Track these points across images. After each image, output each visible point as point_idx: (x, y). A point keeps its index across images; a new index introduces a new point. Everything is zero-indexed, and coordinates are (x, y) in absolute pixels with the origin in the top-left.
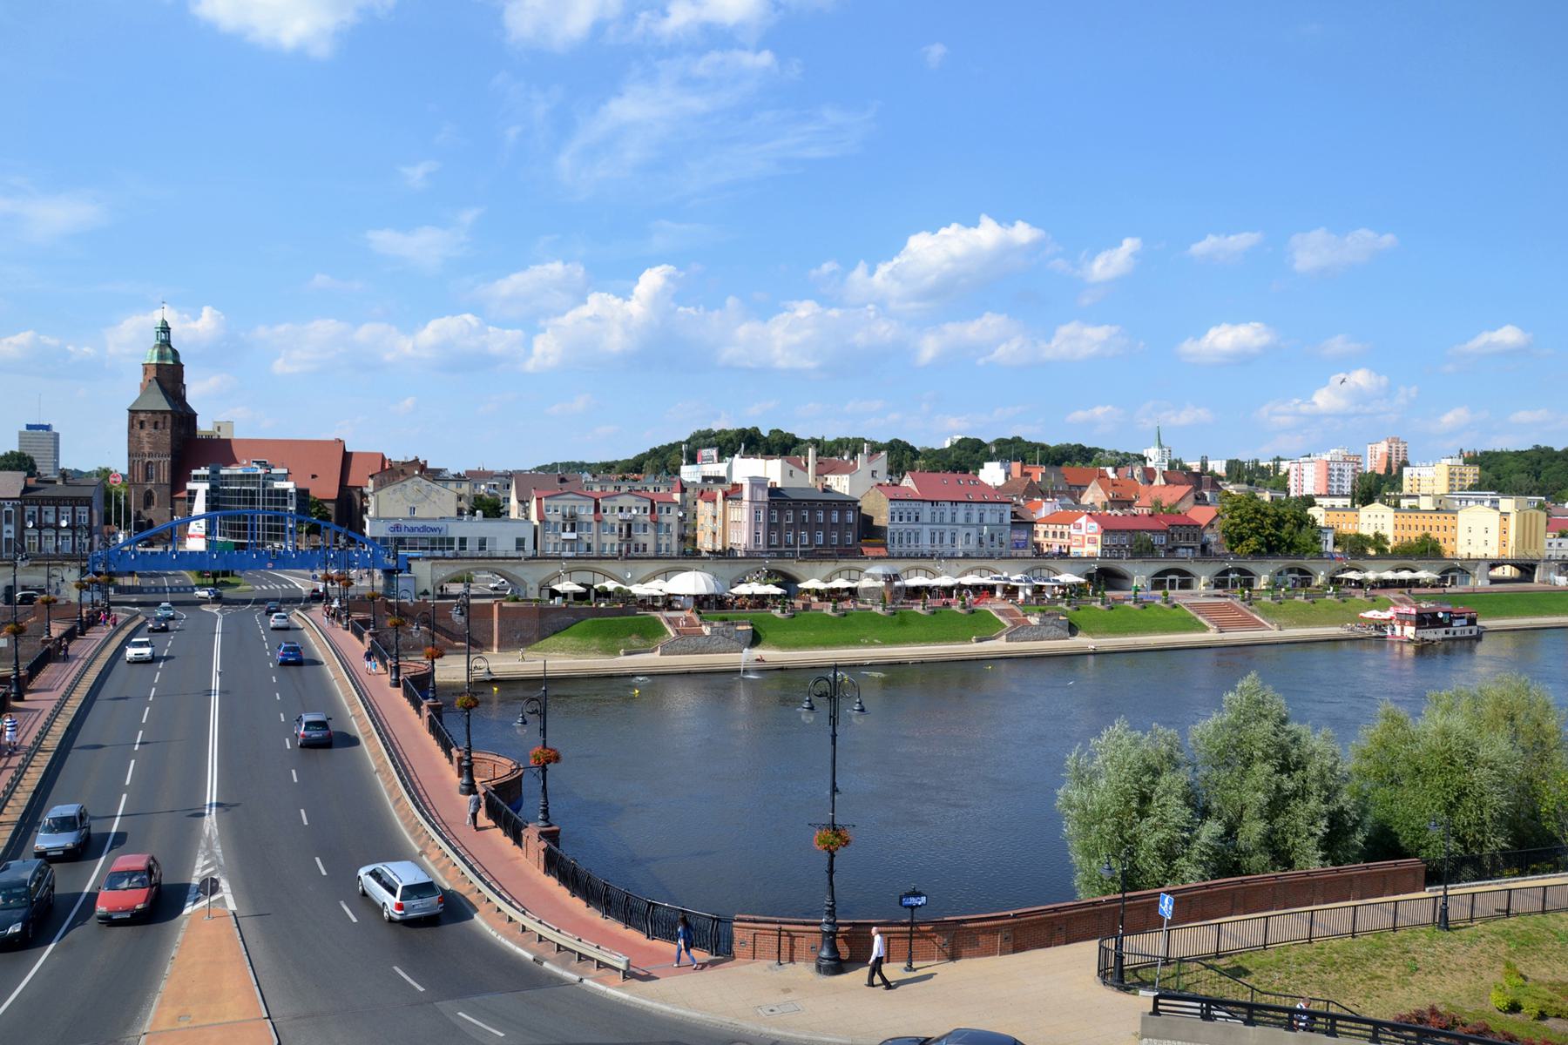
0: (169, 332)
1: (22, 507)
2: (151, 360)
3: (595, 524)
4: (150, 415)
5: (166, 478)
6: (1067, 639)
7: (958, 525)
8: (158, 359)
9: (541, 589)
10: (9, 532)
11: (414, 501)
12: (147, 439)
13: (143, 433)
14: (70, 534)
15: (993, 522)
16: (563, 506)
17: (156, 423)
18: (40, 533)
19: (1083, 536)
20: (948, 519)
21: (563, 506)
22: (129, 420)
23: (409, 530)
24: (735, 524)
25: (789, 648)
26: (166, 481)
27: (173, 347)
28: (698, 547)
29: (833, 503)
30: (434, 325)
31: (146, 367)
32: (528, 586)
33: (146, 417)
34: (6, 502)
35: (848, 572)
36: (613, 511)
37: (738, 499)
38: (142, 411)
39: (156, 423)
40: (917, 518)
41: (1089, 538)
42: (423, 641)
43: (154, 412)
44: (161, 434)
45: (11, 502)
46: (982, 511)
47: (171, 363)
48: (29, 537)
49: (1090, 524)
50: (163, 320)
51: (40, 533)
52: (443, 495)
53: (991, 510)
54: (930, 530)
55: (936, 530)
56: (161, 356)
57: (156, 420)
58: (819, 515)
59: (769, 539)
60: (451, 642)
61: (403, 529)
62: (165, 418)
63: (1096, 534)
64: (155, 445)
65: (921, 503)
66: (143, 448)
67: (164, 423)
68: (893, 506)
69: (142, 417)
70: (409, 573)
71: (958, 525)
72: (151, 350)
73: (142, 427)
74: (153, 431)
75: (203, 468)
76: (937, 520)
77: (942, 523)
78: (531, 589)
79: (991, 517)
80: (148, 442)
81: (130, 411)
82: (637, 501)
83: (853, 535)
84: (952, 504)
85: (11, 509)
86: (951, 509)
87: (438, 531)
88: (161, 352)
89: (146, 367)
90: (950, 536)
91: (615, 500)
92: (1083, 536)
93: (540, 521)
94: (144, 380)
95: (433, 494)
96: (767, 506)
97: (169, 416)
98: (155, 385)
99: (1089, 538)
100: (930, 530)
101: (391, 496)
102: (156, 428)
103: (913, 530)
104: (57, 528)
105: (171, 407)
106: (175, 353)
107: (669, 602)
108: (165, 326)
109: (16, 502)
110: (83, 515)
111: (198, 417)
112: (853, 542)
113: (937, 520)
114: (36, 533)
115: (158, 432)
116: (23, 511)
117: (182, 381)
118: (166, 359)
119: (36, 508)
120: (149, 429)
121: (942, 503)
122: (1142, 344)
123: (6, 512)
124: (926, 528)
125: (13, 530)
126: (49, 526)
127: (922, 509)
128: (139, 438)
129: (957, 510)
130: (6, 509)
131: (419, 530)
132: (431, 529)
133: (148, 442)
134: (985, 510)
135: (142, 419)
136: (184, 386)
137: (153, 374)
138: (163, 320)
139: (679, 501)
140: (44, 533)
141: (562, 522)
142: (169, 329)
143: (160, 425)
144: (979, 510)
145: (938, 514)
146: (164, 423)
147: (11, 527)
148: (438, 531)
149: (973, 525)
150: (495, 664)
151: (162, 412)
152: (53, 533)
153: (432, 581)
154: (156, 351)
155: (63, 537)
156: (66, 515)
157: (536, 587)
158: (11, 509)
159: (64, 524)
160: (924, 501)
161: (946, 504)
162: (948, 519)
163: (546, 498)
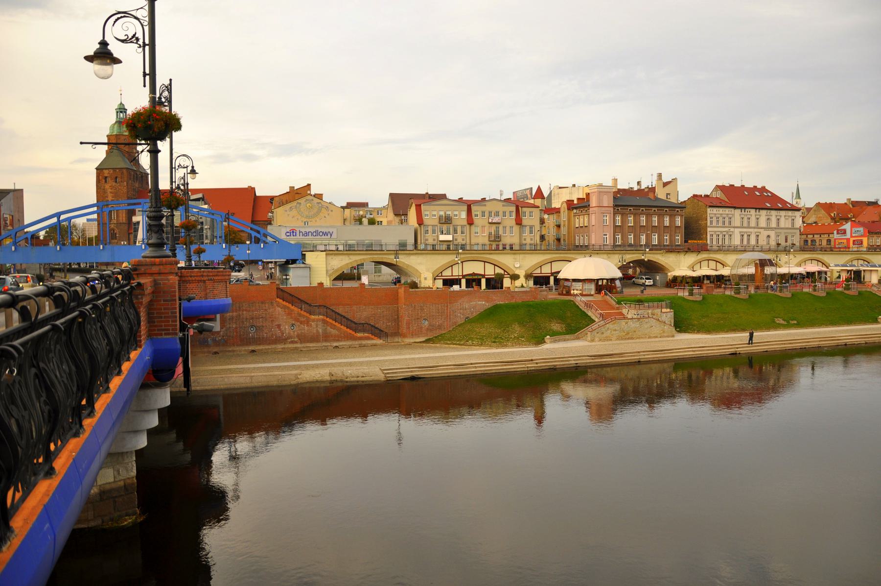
2: (113, 133)
5: (124, 219)
6: (673, 336)
7: (761, 228)
9: (435, 279)
11: (307, 217)
12: (110, 190)
13: (107, 186)
15: (787, 226)
19: (848, 240)
20: (753, 223)
23: (303, 235)
24: (581, 230)
25: (826, 325)
26: (124, 221)
32: (423, 276)
35: (707, 261)
36: (483, 215)
37: (585, 207)
40: (730, 223)
41: (854, 241)
42: (320, 331)
43: (114, 169)
44: (119, 186)
49: (854, 229)
50: (121, 103)
53: (785, 216)
54: (740, 232)
57: (116, 176)
58: (654, 219)
59: (615, 239)
60: (353, 333)
61: (298, 234)
63: (862, 236)
64: (116, 195)
65: (733, 210)
66: (107, 197)
69: (106, 173)
70: (303, 263)
71: (761, 228)
74: (114, 184)
76: (745, 224)
77: (757, 227)
78: (426, 279)
79: (785, 222)
80: (111, 192)
82: (503, 206)
83: (681, 237)
87: (329, 235)
90: (755, 238)
91: (485, 205)
92: (848, 240)
95: (323, 210)
96: (612, 209)
99: (854, 241)
100: (740, 232)
101: (288, 212)
102: (116, 182)
103: (721, 232)
107: (233, 376)
108: (122, 107)
112: (681, 242)
113: (745, 224)
120: (111, 182)
121: (749, 210)
124: (737, 231)
127: (733, 215)
128: (104, 189)
131: (312, 234)
132: (323, 233)
133: (111, 192)
134: (781, 216)
135: (106, 175)
138: (121, 103)
142: (127, 110)
144: (776, 216)
145: (745, 219)
148: (329, 235)
149: (772, 229)
151: (121, 169)
153: (327, 271)
157: (430, 276)
162: (753, 223)
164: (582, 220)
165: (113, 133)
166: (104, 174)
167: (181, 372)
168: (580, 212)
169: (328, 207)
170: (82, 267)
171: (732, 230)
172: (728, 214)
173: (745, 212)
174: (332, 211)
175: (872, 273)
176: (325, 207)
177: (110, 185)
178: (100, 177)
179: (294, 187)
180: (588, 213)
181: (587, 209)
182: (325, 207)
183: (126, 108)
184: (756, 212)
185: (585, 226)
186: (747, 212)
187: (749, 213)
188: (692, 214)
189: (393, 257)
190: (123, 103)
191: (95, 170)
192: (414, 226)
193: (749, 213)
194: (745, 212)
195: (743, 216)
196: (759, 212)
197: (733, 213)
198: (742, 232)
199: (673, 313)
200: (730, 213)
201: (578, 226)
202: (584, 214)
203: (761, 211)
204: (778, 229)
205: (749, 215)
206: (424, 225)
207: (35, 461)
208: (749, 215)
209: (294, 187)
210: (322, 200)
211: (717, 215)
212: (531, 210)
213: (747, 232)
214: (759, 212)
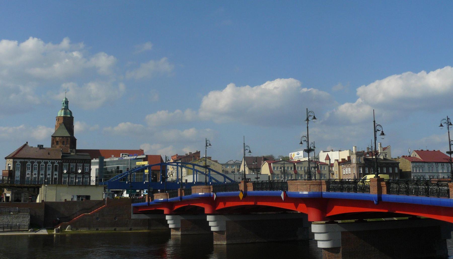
0: (68, 103)
1: (62, 163)
2: (61, 115)
10: (56, 175)
14: (81, 176)
16: (277, 167)
17: (63, 142)
18: (69, 176)
21: (277, 167)
22: (52, 141)
27: (69, 110)
29: (390, 164)
30: (229, 89)
31: (58, 119)
39: (63, 142)
43: (63, 137)
44: (65, 147)
51: (69, 176)
55: (431, 175)
56: (65, 113)
62: (67, 139)
65: (424, 163)
67: (67, 142)
68: (413, 165)
69: (58, 139)
72: (60, 111)
74: (62, 145)
75: (94, 159)
81: (52, 136)
84: (436, 163)
85: (57, 164)
86: (436, 166)
88: (65, 112)
89: (58, 119)
91: (302, 164)
98: (63, 126)
102: (63, 144)
104: (76, 173)
106: (71, 112)
109: (59, 161)
110: (87, 168)
117: (73, 124)
118: (67, 114)
119: (75, 164)
121: (432, 163)
122: (17, 208)
126: (73, 172)
129: (438, 166)
130: (55, 164)
137: (61, 121)
139: (329, 164)
141: (280, 174)
142: (68, 102)
143: (65, 143)
144: (447, 166)
146: (67, 142)
147: (57, 173)
152: (74, 176)
154: (63, 111)
156: (80, 168)
158: (57, 164)
159: (80, 171)
160: (425, 162)
161: (433, 163)
163: (273, 163)
164: (347, 170)
165: (61, 115)
166: (56, 139)
167: (236, 179)
168: (346, 166)
169: (214, 164)
170: (184, 188)
172: (421, 166)
173: (430, 164)
174: (216, 166)
176: (213, 164)
177: (60, 146)
178: (54, 141)
179: (191, 153)
180: (351, 167)
181: (349, 165)
182: (213, 164)
185: (346, 174)
186: (431, 164)
188: (402, 166)
190: (67, 98)
191: (51, 137)
192: (268, 174)
194: (430, 164)
195: (429, 167)
196: (438, 164)
199: (252, 186)
200: (422, 165)
201: (344, 174)
202: (348, 167)
203: (425, 164)
205: (432, 166)
208: (432, 166)
209: (191, 153)
210: (211, 160)
211: (432, 166)
212: (324, 166)
214: (438, 164)
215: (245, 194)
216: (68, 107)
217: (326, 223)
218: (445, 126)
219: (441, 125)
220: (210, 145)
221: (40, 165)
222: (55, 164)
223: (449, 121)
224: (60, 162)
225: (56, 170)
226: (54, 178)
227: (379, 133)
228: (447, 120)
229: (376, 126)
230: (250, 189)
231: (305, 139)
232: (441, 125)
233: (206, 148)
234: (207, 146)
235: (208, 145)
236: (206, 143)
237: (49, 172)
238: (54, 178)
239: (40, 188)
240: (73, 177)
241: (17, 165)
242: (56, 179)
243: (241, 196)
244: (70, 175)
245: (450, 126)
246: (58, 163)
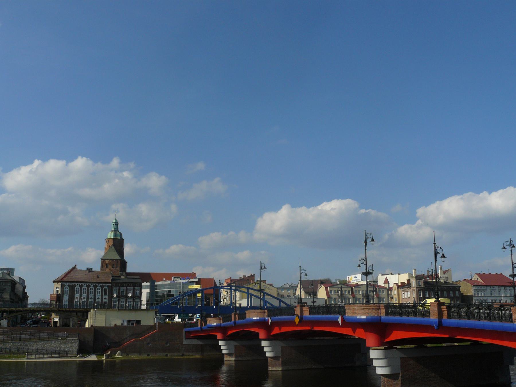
0: (118, 225)
3: (352, 298)
4: (111, 261)
8: (114, 236)
10: (105, 299)
21: (334, 291)
28: (461, 292)
30: (285, 210)
33: (109, 262)
34: (105, 285)
38: (107, 259)
44: (115, 270)
45: (107, 285)
46: (511, 290)
47: (119, 238)
48: (114, 301)
51: (119, 300)
52: (271, 290)
56: (115, 235)
65: (486, 287)
67: (117, 265)
68: (475, 289)
69: (107, 262)
73: (107, 267)
74: (112, 268)
81: (102, 259)
85: (107, 288)
88: (115, 233)
89: (108, 241)
91: (360, 287)
93: (328, 298)
94: (107, 246)
97: (119, 261)
98: (113, 248)
104: (127, 297)
105: (120, 258)
106: (121, 234)
109: (109, 285)
110: (137, 291)
111: (127, 263)
114: (117, 299)
115: (114, 269)
116: (112, 288)
118: (117, 236)
121: (495, 287)
123: (105, 289)
125: (107, 298)
126: (123, 296)
129: (501, 290)
130: (105, 288)
135: (107, 263)
136: (124, 248)
137: (111, 243)
140: (121, 300)
142: (118, 223)
144: (510, 290)
146: (117, 265)
147: (107, 297)
150: (274, 369)
152: (124, 300)
154: (113, 233)
155: (129, 302)
158: (107, 288)
159: (130, 295)
160: (487, 286)
164: (406, 294)
165: (111, 237)
169: (269, 288)
171: (486, 298)
172: (483, 290)
175: (263, 314)
177: (109, 269)
178: (104, 264)
181: (409, 288)
183: (118, 222)
184: (490, 288)
185: (406, 298)
187: (494, 288)
189: (267, 315)
193: (494, 288)
196: (500, 288)
197: (486, 289)
198: (511, 299)
200: (484, 289)
201: (404, 298)
203: (501, 287)
204: (511, 297)
206: (345, 298)
207: (181, 322)
210: (266, 283)
213: (494, 299)
214: (500, 288)
215: (301, 319)
216: (118, 229)
217: (385, 349)
218: (508, 248)
219: (504, 248)
220: (265, 268)
221: (83, 288)
222: (105, 288)
223: (512, 243)
224: (110, 285)
225: (105, 294)
226: (103, 302)
227: (439, 256)
228: (510, 242)
229: (436, 248)
230: (306, 313)
231: (363, 261)
232: (504, 248)
233: (261, 271)
234: (261, 269)
235: (263, 267)
236: (261, 266)
237: (99, 296)
238: (104, 302)
239: (89, 313)
240: (123, 302)
241: (65, 288)
242: (105, 303)
243: (297, 320)
244: (120, 299)
245: (513, 248)
246: (108, 286)
